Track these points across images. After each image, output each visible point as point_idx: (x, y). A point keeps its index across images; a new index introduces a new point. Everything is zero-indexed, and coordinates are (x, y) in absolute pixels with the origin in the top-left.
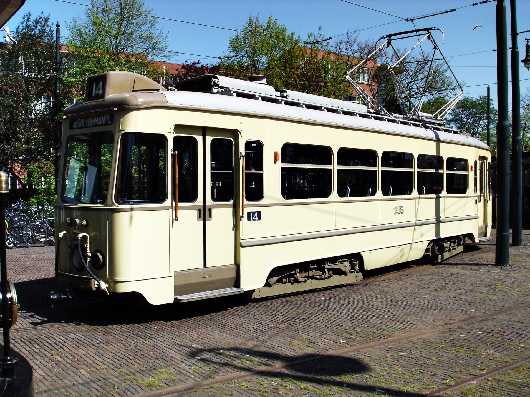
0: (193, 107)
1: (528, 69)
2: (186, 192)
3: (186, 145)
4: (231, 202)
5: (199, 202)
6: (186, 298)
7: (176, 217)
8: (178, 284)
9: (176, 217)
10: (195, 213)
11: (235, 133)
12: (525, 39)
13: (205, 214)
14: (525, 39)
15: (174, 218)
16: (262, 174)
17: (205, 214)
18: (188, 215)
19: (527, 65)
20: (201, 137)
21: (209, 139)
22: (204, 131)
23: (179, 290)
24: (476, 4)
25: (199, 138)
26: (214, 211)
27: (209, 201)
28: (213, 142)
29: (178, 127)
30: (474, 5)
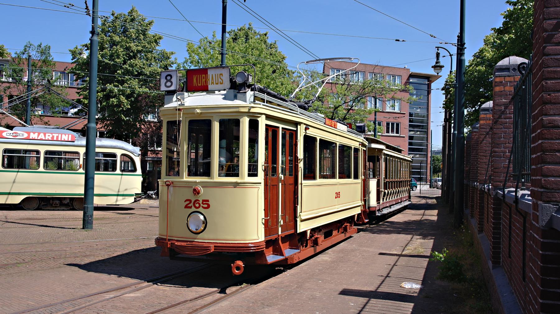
19: (437, 71)
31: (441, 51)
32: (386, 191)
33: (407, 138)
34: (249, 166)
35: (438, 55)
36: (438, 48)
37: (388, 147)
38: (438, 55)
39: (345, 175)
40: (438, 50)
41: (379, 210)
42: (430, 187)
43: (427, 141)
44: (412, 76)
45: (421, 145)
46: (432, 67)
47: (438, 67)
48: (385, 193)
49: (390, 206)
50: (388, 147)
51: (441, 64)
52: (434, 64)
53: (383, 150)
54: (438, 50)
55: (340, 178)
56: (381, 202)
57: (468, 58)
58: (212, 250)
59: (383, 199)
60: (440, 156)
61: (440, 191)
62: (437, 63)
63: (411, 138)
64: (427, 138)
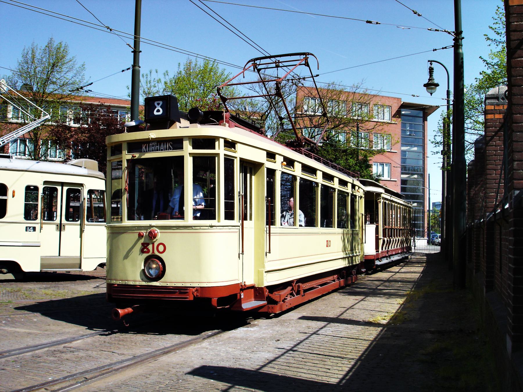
0: (14, 169)
1: (431, 94)
2: (50, 216)
3: (50, 191)
4: (79, 222)
5: (58, 221)
6: (45, 270)
7: (243, 251)
8: (43, 262)
9: (243, 251)
10: (55, 227)
11: (81, 185)
12: (429, 61)
13: (60, 228)
14: (429, 61)
15: (241, 252)
16: (25, 201)
17: (60, 228)
18: (50, 228)
19: (430, 91)
20: (60, 187)
21: (65, 188)
22: (62, 184)
23: (42, 266)
24: (436, 50)
25: (59, 188)
26: (66, 227)
27: (64, 221)
28: (68, 190)
29: (45, 182)
30: (434, 50)
31: (434, 65)
32: (385, 239)
33: (399, 183)
34: (226, 204)
35: (431, 70)
36: (431, 62)
37: (387, 191)
38: (431, 70)
39: (327, 223)
40: (431, 64)
41: (378, 259)
42: (429, 243)
43: (424, 185)
44: (405, 106)
45: (414, 190)
46: (425, 85)
47: (431, 86)
48: (384, 241)
49: (390, 256)
50: (387, 191)
51: (436, 82)
52: (426, 82)
53: (382, 193)
54: (431, 64)
55: (322, 226)
56: (380, 250)
57: (471, 79)
58: (191, 298)
59: (382, 249)
60: (439, 209)
61: (439, 248)
62: (429, 80)
63: (404, 182)
64: (424, 182)
